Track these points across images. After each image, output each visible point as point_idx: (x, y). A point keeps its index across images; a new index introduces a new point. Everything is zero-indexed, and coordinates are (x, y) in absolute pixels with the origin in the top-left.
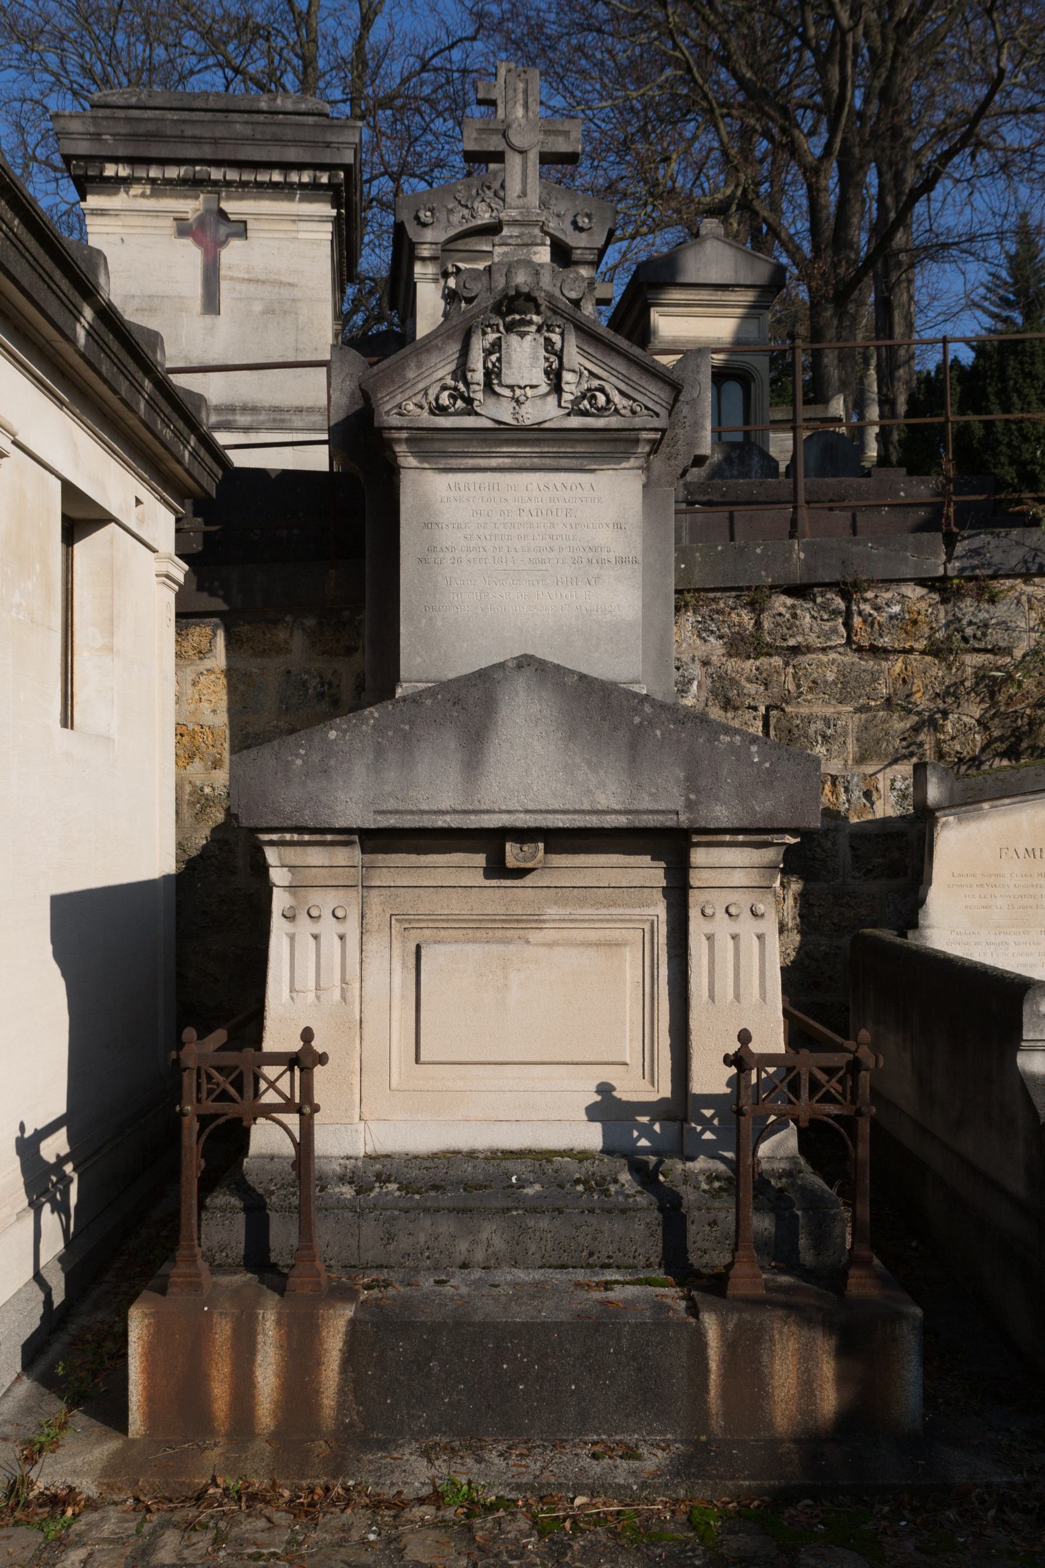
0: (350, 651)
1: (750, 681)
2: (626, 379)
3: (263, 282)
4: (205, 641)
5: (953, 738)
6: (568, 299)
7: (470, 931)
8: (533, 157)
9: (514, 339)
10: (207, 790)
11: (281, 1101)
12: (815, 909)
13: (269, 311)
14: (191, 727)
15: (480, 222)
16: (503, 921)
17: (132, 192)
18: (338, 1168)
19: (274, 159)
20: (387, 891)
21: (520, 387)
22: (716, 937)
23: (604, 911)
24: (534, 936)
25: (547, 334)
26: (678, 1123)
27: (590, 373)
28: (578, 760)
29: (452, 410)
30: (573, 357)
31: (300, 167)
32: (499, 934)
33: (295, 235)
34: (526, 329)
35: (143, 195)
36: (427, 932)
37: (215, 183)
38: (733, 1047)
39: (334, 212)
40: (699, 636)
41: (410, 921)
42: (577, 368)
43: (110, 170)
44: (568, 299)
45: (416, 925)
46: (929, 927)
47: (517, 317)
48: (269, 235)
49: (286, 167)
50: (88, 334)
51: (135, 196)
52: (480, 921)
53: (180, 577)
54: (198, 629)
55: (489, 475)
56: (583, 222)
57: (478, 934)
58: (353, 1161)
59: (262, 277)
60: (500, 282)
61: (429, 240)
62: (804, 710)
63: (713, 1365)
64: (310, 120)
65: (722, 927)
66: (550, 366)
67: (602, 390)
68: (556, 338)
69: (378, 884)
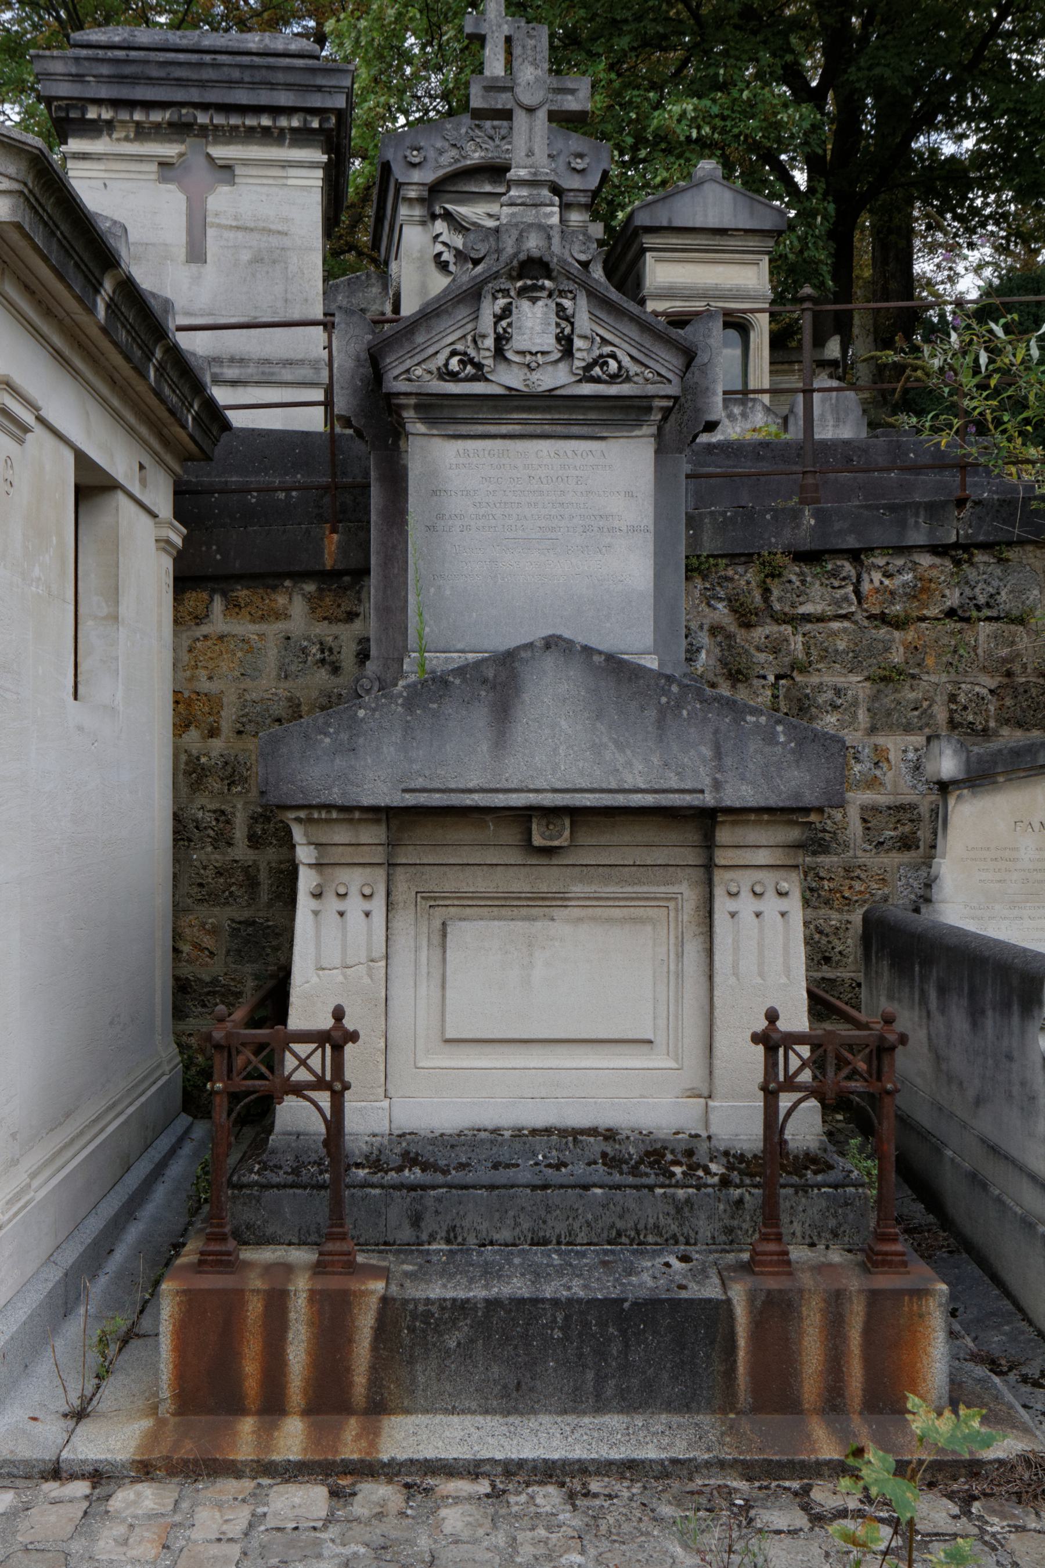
0: (351, 616)
1: (759, 649)
2: (639, 347)
3: (252, 230)
4: (201, 607)
5: (965, 708)
6: (578, 261)
7: (495, 909)
8: (542, 114)
9: (525, 305)
10: (203, 760)
11: (311, 1078)
12: (826, 883)
13: (257, 260)
14: (186, 694)
15: (469, 162)
16: (529, 899)
17: (115, 136)
18: (364, 1147)
19: (262, 103)
20: (412, 869)
21: (531, 353)
22: (741, 915)
23: (629, 889)
24: (556, 913)
25: (559, 300)
26: (702, 1100)
27: (602, 338)
28: (605, 739)
29: (462, 375)
30: (584, 322)
31: (289, 111)
32: (524, 911)
33: (285, 181)
34: (538, 294)
35: (127, 139)
36: (452, 910)
37: (203, 128)
38: (761, 1024)
39: (324, 158)
40: (709, 605)
41: (435, 899)
42: (588, 333)
43: (92, 114)
44: (578, 261)
45: (441, 903)
46: (942, 902)
47: (529, 282)
48: (258, 181)
49: (276, 111)
50: (108, 307)
51: (118, 140)
52: (505, 898)
53: (178, 541)
54: (194, 594)
55: (499, 443)
56: (579, 164)
57: (504, 911)
58: (379, 1138)
59: (252, 225)
60: (509, 246)
61: (415, 180)
62: (815, 679)
63: (742, 1343)
64: (300, 62)
65: (746, 905)
66: (562, 332)
67: (613, 356)
68: (567, 303)
69: (404, 861)
